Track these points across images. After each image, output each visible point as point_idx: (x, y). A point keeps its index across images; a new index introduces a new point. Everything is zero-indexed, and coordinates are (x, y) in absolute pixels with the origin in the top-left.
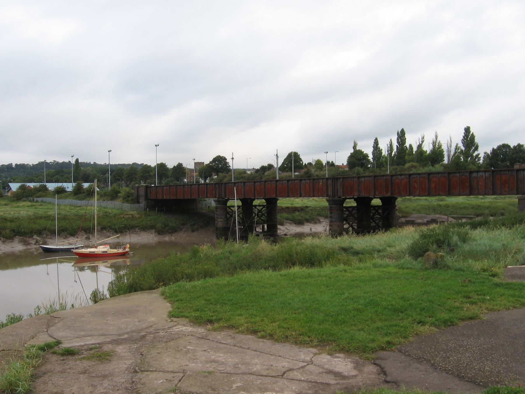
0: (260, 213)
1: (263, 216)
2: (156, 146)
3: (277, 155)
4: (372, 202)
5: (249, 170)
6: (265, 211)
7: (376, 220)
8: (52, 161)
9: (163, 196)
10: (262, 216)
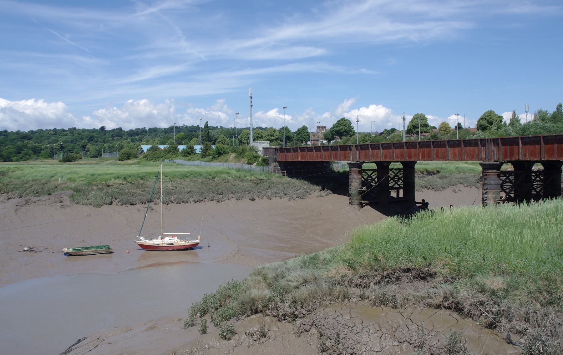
0: (397, 178)
1: (373, 182)
2: (284, 108)
3: (404, 117)
4: (502, 167)
5: (374, 133)
6: (402, 175)
7: (538, 187)
8: (182, 126)
9: (293, 159)
10: (398, 180)
